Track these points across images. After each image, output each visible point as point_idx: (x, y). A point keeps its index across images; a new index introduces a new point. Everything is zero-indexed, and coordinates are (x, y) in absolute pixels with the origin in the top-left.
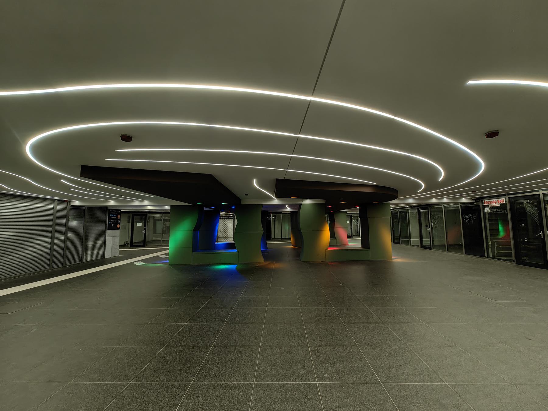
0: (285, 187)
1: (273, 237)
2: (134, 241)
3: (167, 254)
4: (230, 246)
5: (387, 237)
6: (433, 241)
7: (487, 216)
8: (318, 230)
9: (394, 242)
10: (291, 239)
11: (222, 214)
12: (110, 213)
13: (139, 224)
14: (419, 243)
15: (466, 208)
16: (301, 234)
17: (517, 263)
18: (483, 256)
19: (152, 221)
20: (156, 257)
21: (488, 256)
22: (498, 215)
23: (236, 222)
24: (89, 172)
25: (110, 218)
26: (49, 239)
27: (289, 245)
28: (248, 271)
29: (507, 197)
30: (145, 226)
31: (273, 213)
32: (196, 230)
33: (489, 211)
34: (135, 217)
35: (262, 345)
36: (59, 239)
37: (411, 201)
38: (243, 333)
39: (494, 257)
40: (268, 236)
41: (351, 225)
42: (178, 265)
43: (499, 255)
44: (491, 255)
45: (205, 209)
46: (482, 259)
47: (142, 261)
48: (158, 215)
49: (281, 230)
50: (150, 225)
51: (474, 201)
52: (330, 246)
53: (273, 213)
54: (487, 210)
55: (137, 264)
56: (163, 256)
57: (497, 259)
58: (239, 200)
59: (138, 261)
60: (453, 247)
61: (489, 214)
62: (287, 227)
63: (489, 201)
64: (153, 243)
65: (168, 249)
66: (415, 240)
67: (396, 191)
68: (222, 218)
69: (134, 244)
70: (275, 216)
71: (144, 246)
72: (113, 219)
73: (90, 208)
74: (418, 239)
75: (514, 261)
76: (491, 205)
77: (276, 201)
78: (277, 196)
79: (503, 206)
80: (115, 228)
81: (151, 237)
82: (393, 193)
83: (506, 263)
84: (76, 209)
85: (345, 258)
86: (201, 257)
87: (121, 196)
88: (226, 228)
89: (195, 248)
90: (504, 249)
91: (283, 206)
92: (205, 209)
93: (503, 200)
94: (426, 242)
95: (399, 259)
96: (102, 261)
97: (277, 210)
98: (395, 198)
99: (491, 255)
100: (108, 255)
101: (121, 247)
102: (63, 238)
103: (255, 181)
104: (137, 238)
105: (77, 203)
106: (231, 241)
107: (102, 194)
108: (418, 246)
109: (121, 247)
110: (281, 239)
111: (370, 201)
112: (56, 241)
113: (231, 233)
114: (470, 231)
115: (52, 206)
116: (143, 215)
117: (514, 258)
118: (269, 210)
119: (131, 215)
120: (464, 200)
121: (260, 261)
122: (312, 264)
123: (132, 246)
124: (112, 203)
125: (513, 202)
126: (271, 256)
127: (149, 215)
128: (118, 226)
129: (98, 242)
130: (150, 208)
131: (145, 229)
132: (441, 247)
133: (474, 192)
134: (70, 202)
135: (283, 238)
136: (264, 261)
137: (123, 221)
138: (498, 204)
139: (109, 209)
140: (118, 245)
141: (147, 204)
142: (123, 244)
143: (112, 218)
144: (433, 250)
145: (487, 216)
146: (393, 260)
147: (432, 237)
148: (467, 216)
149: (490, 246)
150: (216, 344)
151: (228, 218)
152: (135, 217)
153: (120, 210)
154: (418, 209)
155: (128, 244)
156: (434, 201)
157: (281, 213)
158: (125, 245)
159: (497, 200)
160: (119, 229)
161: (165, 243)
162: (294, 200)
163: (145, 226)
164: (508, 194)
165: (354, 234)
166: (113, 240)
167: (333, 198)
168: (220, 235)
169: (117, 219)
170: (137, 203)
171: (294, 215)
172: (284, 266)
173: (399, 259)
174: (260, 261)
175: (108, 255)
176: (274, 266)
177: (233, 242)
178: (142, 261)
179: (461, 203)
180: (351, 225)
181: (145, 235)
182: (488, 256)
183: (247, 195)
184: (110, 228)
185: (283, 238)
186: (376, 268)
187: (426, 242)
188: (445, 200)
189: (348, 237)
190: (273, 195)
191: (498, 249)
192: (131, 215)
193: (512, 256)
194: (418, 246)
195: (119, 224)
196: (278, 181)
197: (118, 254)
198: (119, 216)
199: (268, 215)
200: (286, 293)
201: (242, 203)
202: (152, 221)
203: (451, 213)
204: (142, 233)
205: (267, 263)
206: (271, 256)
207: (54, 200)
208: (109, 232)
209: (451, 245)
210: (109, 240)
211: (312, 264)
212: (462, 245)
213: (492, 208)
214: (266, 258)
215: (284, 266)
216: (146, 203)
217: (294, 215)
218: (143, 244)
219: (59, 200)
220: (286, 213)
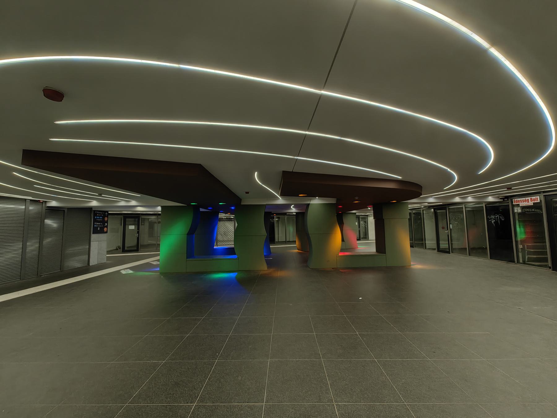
0: (295, 183)
1: (276, 240)
2: (126, 245)
3: (158, 260)
4: (230, 251)
5: (404, 239)
6: (452, 244)
7: (517, 217)
8: (327, 234)
9: (412, 246)
10: (297, 243)
11: (222, 215)
12: (95, 215)
13: (132, 227)
14: (435, 246)
15: (492, 208)
16: (309, 238)
17: (553, 270)
18: (514, 262)
19: (147, 224)
20: (148, 264)
21: (518, 262)
22: (531, 216)
23: (236, 225)
24: (35, 158)
25: (95, 221)
26: (20, 245)
27: (294, 249)
28: (250, 281)
29: (542, 195)
30: (138, 229)
31: (277, 214)
32: (190, 233)
33: (520, 211)
34: (127, 219)
35: (267, 402)
36: (32, 246)
37: (431, 200)
38: (240, 378)
39: (524, 263)
40: (271, 239)
41: (359, 227)
42: (171, 275)
43: (530, 260)
44: (521, 261)
45: (201, 210)
46: (511, 265)
47: (131, 268)
48: (154, 217)
49: (286, 232)
50: (145, 228)
51: (502, 200)
52: (342, 250)
53: (277, 214)
54: (518, 210)
55: (123, 272)
56: (155, 263)
57: (527, 264)
58: (240, 200)
59: (125, 269)
60: (475, 250)
61: (519, 214)
62: (292, 230)
63: (518, 199)
64: (148, 247)
65: (158, 255)
66: (430, 241)
67: (419, 187)
68: (221, 220)
69: (127, 248)
70: (278, 218)
71: (137, 250)
72: (98, 222)
73: (70, 209)
74: (435, 242)
75: (550, 268)
76: (522, 204)
77: (281, 201)
78: (282, 195)
79: (537, 206)
80: (102, 231)
81: (145, 239)
82: (412, 190)
83: (533, 268)
84: (53, 210)
85: (357, 265)
86: (196, 265)
87: (100, 195)
88: (226, 231)
89: (190, 254)
90: (535, 253)
91: (288, 206)
92: (201, 210)
93: (537, 199)
94: (444, 245)
95: (420, 265)
96: (87, 269)
97: (281, 211)
98: (417, 195)
99: (521, 261)
100: (93, 262)
101: (109, 252)
102: (37, 245)
103: (256, 173)
104: (130, 242)
105: (54, 204)
106: (231, 245)
107: (77, 192)
108: (435, 249)
109: (109, 252)
110: (286, 242)
111: (385, 200)
112: (29, 249)
113: (231, 236)
114: (496, 234)
115: (24, 207)
116: (136, 218)
117: (550, 264)
118: (273, 211)
119: (122, 216)
120: (491, 199)
121: (263, 268)
122: (323, 272)
123: (124, 251)
124: (94, 203)
125: (548, 200)
126: (275, 262)
127: (143, 217)
128: (105, 229)
129: (81, 247)
130: (140, 209)
131: (138, 232)
132: (462, 250)
133: (509, 188)
134: (46, 202)
135: (287, 242)
136: (268, 268)
137: (113, 224)
138: (531, 203)
139: (94, 211)
140: (106, 250)
141: (134, 203)
142: (115, 248)
143: (99, 220)
144: (451, 254)
145: (517, 217)
146: (412, 267)
147: (450, 239)
148: (493, 217)
149: (520, 250)
150: (201, 401)
151: (229, 220)
152: (127, 219)
153: (107, 212)
154: (434, 209)
155: (120, 248)
156: (457, 200)
157: (285, 214)
158: (117, 249)
159: (529, 198)
160: (106, 232)
161: (157, 247)
162: (302, 200)
163: (138, 229)
164: (544, 192)
165: (362, 236)
166: (99, 246)
167: (346, 195)
168: (220, 237)
169: (104, 222)
170: (122, 203)
171: (301, 217)
172: (290, 274)
173: (420, 265)
174: (263, 268)
175: (93, 262)
176: (280, 274)
177: (233, 246)
178: (131, 268)
179: (485, 202)
180: (359, 227)
181: (138, 239)
182: (518, 262)
183: (247, 193)
184: (96, 232)
185: (287, 242)
186: (394, 277)
187: (444, 245)
188: (470, 199)
189: (358, 240)
190: (278, 193)
191: (529, 253)
192: (122, 216)
193: (547, 261)
194: (435, 249)
195: (107, 227)
196: (285, 174)
197: (105, 261)
198: (106, 219)
199: (271, 216)
200: (293, 301)
201: (242, 204)
202: (147, 224)
203: (475, 212)
204: (135, 237)
205: (271, 270)
206: (275, 262)
207: (26, 200)
208: (94, 236)
209: (473, 249)
210: (94, 246)
211: (323, 272)
212: (486, 248)
213: (523, 208)
214: (270, 264)
215: (290, 274)
216: (133, 203)
217: (301, 217)
218: (136, 249)
219: (31, 200)
220: (290, 215)
